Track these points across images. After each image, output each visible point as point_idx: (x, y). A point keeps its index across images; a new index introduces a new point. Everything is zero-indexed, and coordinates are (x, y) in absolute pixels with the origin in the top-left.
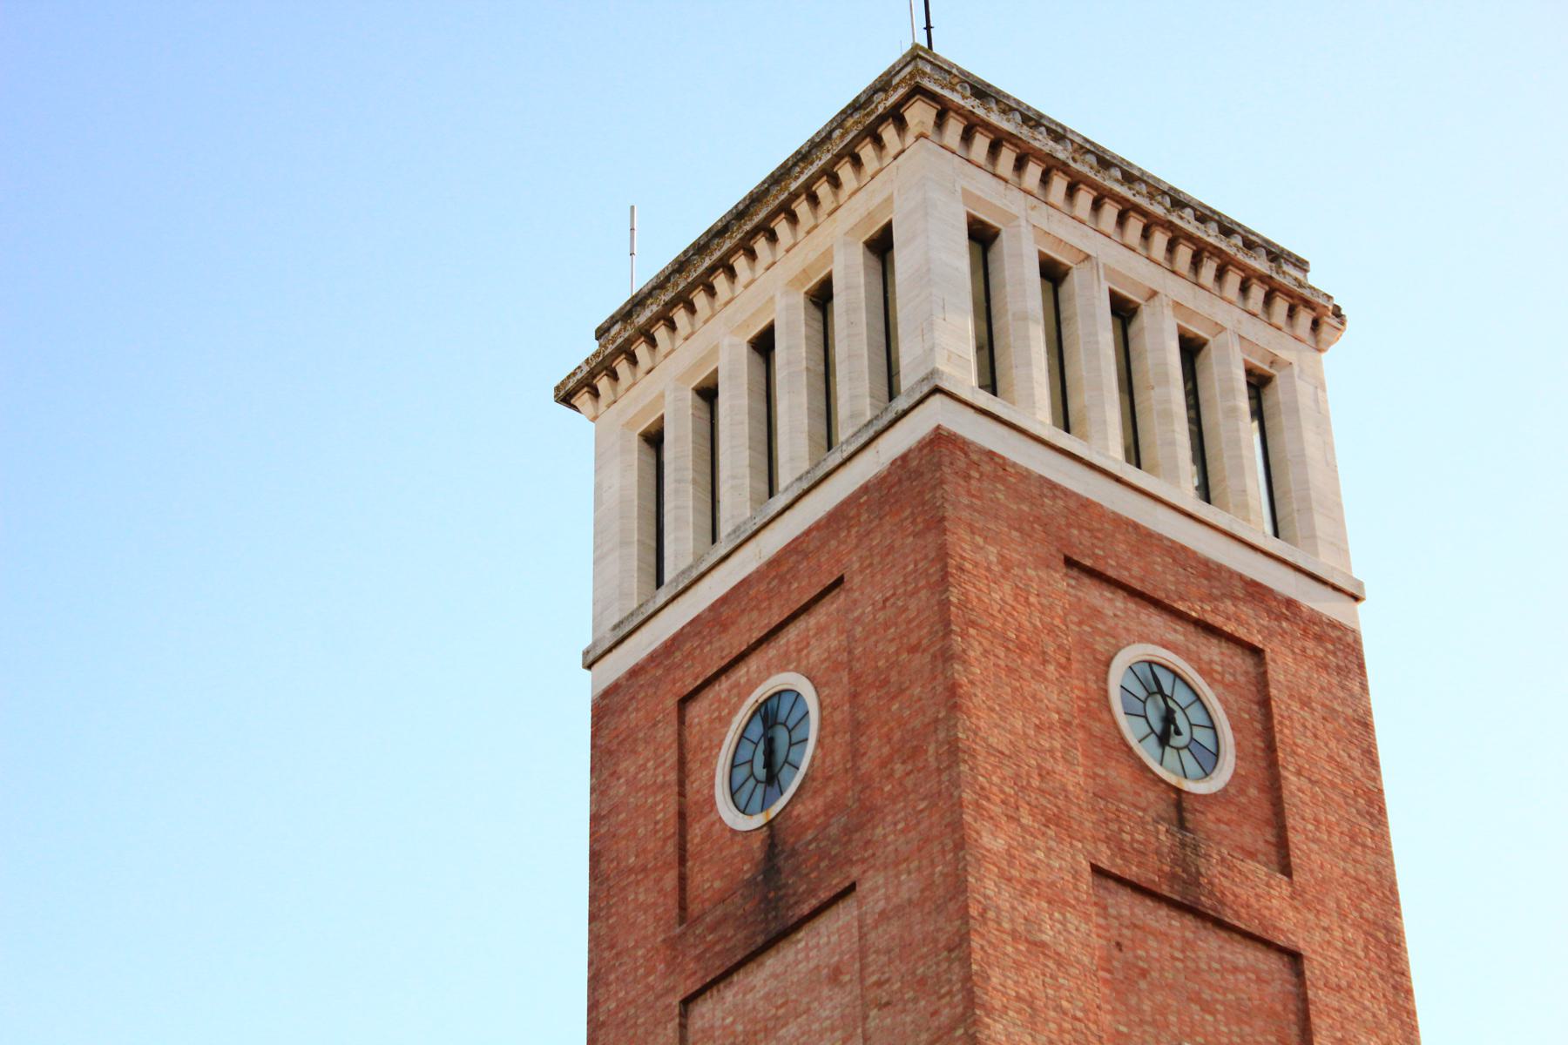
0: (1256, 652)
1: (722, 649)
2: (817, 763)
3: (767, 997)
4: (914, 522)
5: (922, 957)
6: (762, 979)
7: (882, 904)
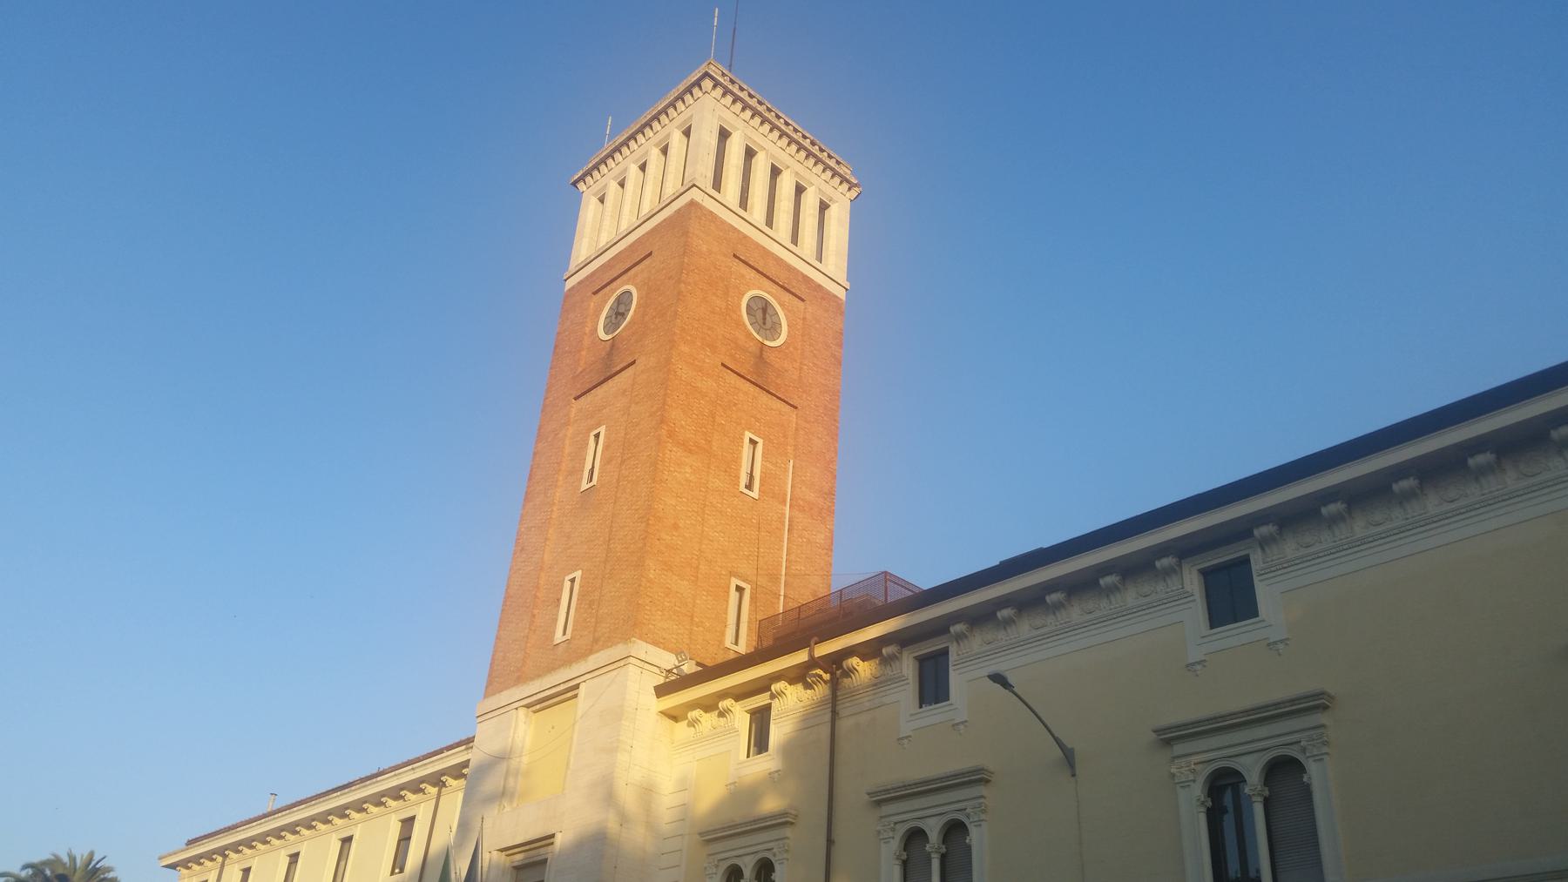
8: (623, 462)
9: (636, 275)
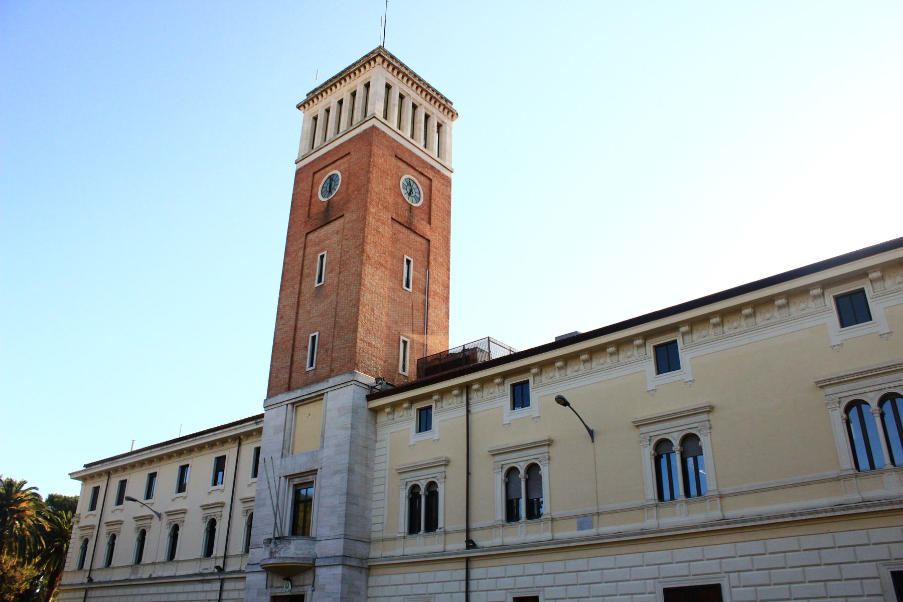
0: (431, 180)
8: (340, 273)
9: (340, 165)
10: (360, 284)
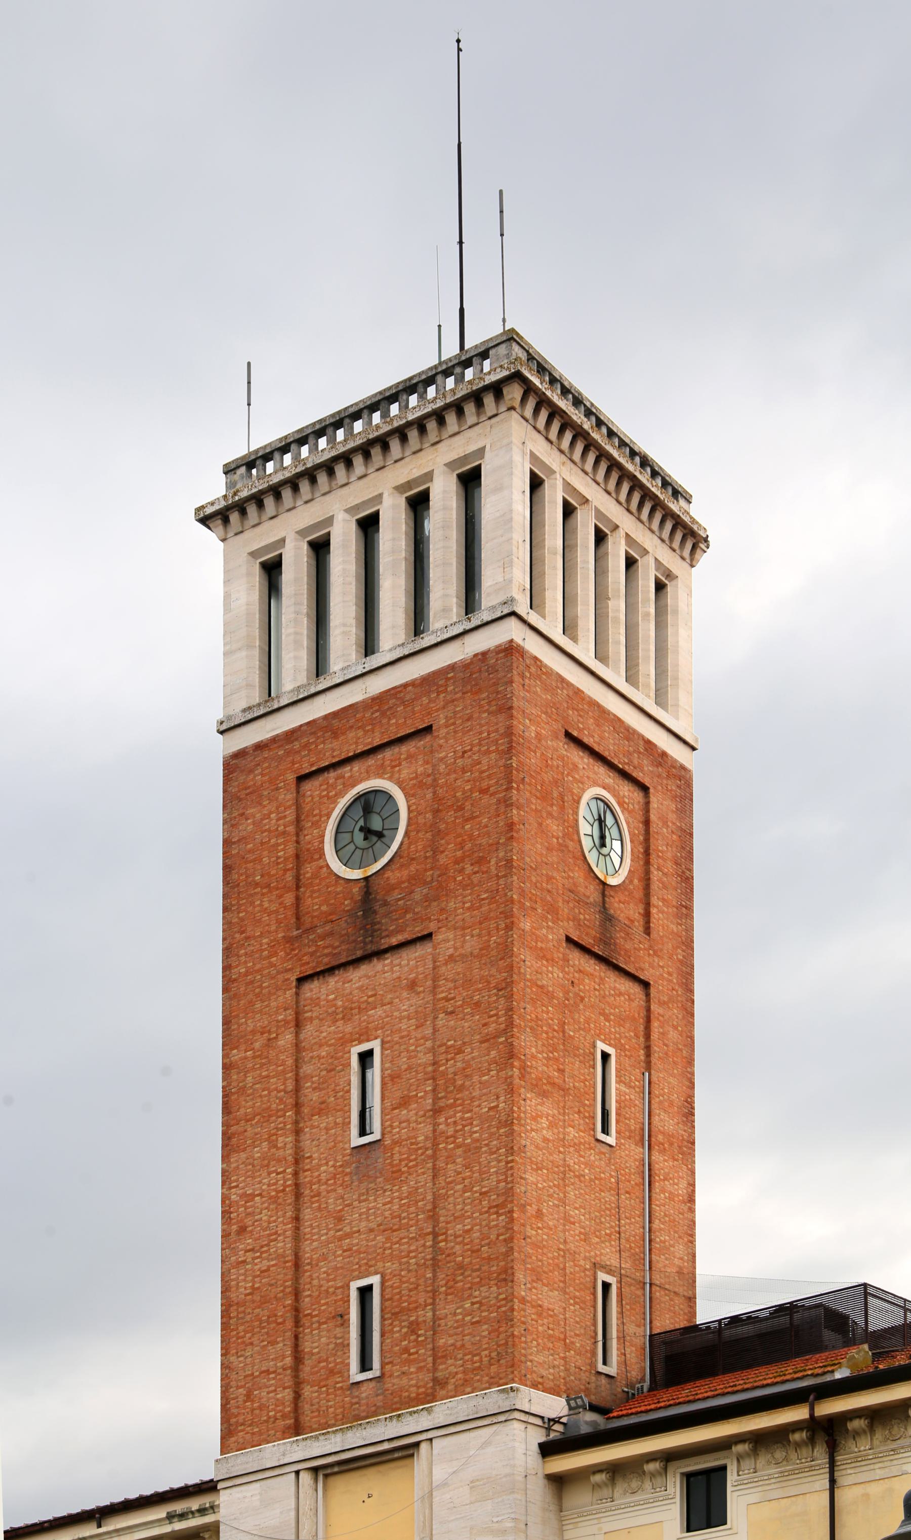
0: (645, 789)
1: (333, 750)
2: (405, 847)
3: (360, 988)
4: (489, 703)
5: (478, 990)
6: (358, 976)
7: (451, 951)
8: (437, 1111)
10: (511, 1151)
